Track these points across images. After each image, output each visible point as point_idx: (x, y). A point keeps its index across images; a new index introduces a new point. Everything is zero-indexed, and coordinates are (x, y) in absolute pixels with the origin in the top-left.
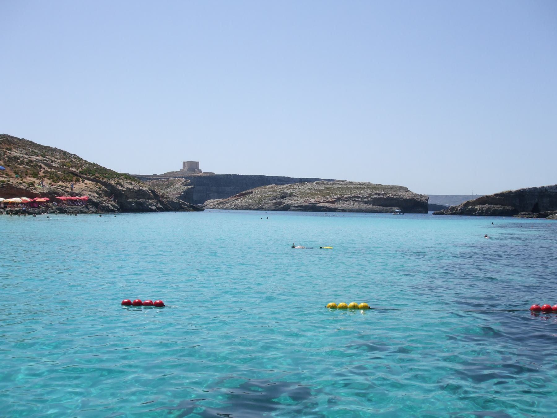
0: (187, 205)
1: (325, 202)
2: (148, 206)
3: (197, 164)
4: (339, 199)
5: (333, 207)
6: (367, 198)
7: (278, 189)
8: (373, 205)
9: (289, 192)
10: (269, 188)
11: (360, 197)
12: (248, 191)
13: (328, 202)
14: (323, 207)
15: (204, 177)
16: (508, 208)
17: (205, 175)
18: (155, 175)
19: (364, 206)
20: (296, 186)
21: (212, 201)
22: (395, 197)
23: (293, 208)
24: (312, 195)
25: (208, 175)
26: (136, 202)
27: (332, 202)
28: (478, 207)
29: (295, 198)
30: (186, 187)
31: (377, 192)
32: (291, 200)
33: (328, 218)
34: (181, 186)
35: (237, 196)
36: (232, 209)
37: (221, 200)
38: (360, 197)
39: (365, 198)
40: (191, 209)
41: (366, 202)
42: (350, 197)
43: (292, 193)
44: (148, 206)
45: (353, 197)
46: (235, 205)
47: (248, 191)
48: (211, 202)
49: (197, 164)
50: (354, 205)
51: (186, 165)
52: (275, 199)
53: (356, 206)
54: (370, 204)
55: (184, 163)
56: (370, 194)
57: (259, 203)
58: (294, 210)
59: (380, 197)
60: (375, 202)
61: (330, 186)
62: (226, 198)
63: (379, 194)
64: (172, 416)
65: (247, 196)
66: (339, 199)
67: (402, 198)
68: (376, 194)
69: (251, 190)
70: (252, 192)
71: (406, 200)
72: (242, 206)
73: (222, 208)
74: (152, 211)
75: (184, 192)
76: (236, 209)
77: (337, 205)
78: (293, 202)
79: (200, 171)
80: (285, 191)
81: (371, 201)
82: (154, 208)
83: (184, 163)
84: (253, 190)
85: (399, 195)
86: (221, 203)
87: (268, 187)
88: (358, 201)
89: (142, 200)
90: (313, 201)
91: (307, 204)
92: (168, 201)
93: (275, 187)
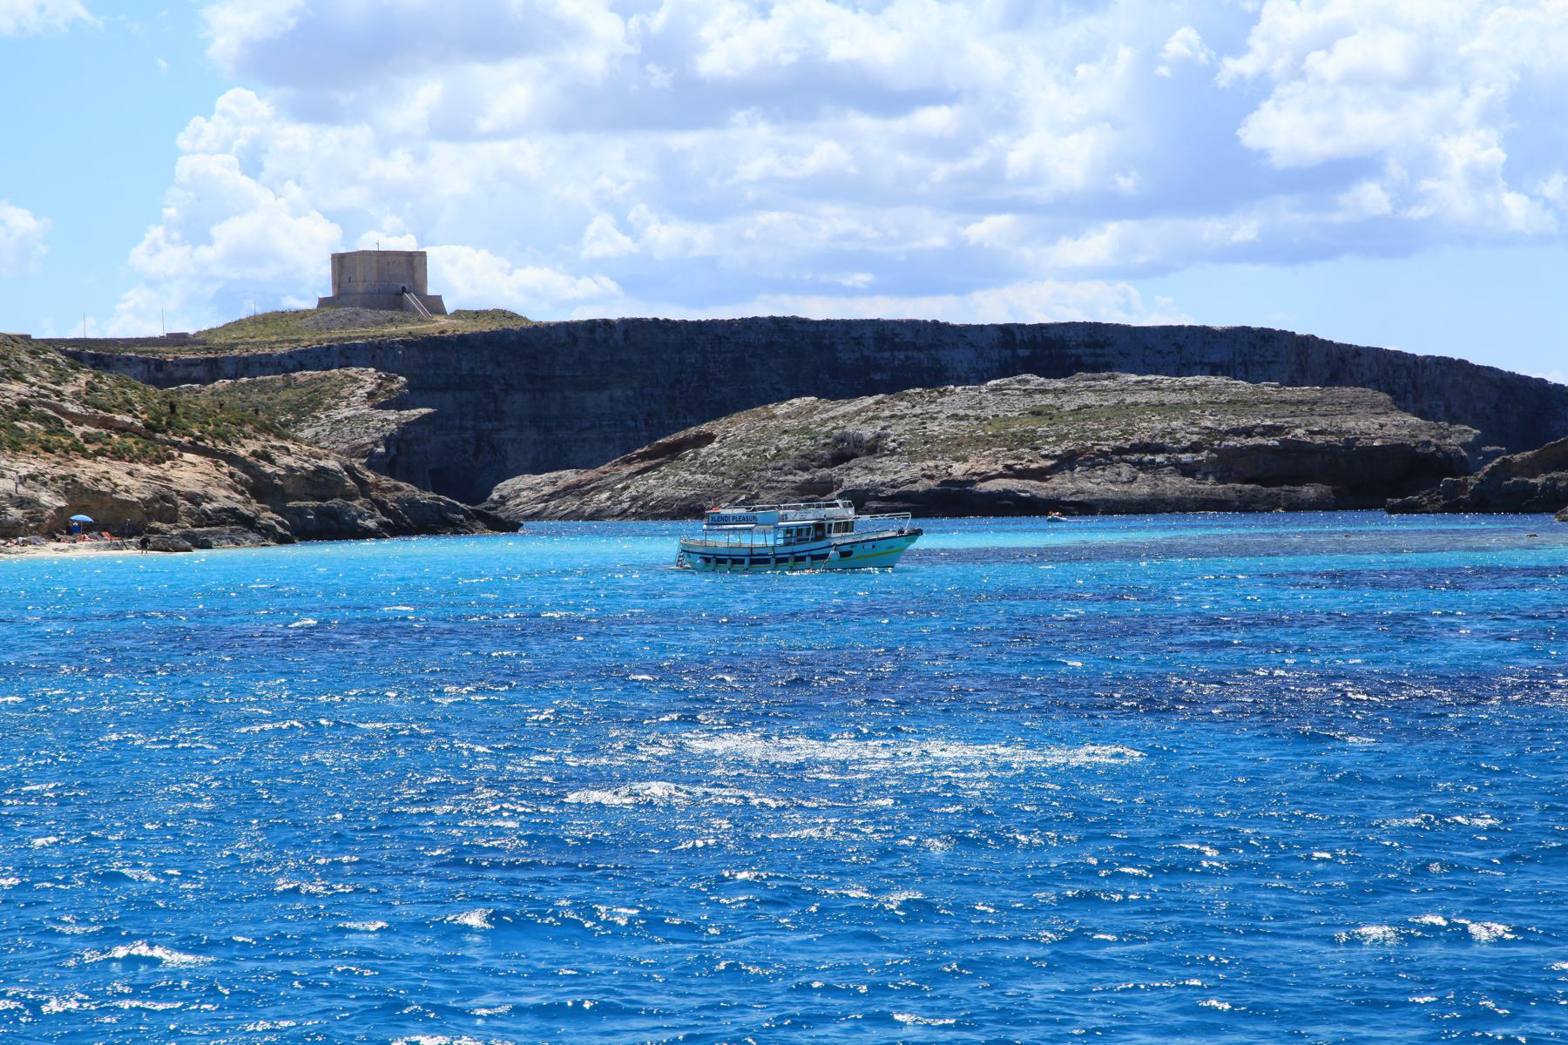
0: (463, 511)
1: (1011, 472)
2: (354, 519)
3: (413, 262)
4: (1067, 462)
5: (1042, 494)
6: (1195, 448)
7: (824, 422)
8: (1221, 480)
9: (868, 432)
10: (788, 416)
11: (1160, 449)
12: (693, 431)
14: (1007, 494)
15: (463, 342)
17: (468, 328)
19: (1173, 485)
20: (902, 406)
21: (528, 480)
22: (1319, 440)
23: (874, 504)
24: (956, 446)
25: (486, 327)
26: (317, 510)
27: (1041, 475)
29: (886, 462)
30: (392, 415)
31: (1243, 422)
32: (871, 470)
34: (365, 409)
35: (643, 457)
36: (623, 514)
37: (569, 476)
38: (1160, 449)
39: (1184, 450)
40: (479, 524)
41: (1186, 470)
42: (1119, 451)
43: (879, 437)
44: (354, 519)
45: (1135, 449)
46: (634, 499)
47: (693, 431)
48: (521, 489)
49: (413, 262)
50: (1133, 480)
52: (805, 469)
53: (1142, 488)
54: (1205, 476)
56: (1211, 432)
57: (736, 485)
59: (1250, 442)
60: (1228, 465)
61: (1049, 400)
62: (589, 465)
63: (1248, 432)
65: (690, 453)
66: (1067, 462)
67: (1350, 443)
68: (1236, 432)
69: (704, 428)
70: (709, 438)
72: (663, 502)
73: (576, 515)
74: (365, 534)
75: (387, 441)
76: (640, 516)
77: (1063, 485)
78: (878, 478)
79: (435, 305)
80: (850, 429)
81: (1210, 461)
82: (371, 524)
84: (716, 427)
85: (1340, 433)
86: (568, 490)
87: (782, 409)
88: (1153, 467)
89: (334, 503)
90: (958, 470)
91: (932, 484)
92: (398, 500)
93: (812, 409)
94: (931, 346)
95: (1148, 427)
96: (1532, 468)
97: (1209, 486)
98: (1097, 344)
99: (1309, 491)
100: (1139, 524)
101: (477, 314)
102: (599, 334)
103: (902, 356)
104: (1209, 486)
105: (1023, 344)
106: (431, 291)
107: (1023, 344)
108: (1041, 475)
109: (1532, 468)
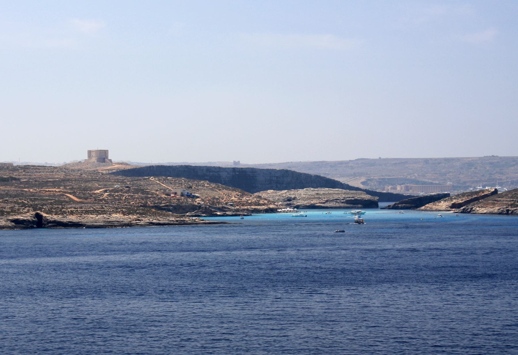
3: (106, 152)
6: (343, 200)
13: (321, 203)
16: (413, 205)
18: (11, 165)
27: (324, 203)
28: (400, 205)
33: (58, 230)
41: (343, 203)
49: (106, 152)
51: (93, 154)
53: (337, 205)
55: (90, 152)
56: (345, 198)
58: (302, 208)
60: (348, 202)
64: (36, 354)
66: (327, 201)
71: (365, 200)
77: (327, 205)
83: (90, 152)
94: (218, 172)
95: (336, 197)
96: (399, 204)
97: (346, 205)
98: (253, 172)
99: (360, 206)
100: (55, 233)
101: (122, 164)
102: (151, 169)
103: (212, 173)
104: (346, 205)
105: (237, 172)
106: (109, 158)
107: (237, 172)
108: (324, 203)
109: (399, 204)
